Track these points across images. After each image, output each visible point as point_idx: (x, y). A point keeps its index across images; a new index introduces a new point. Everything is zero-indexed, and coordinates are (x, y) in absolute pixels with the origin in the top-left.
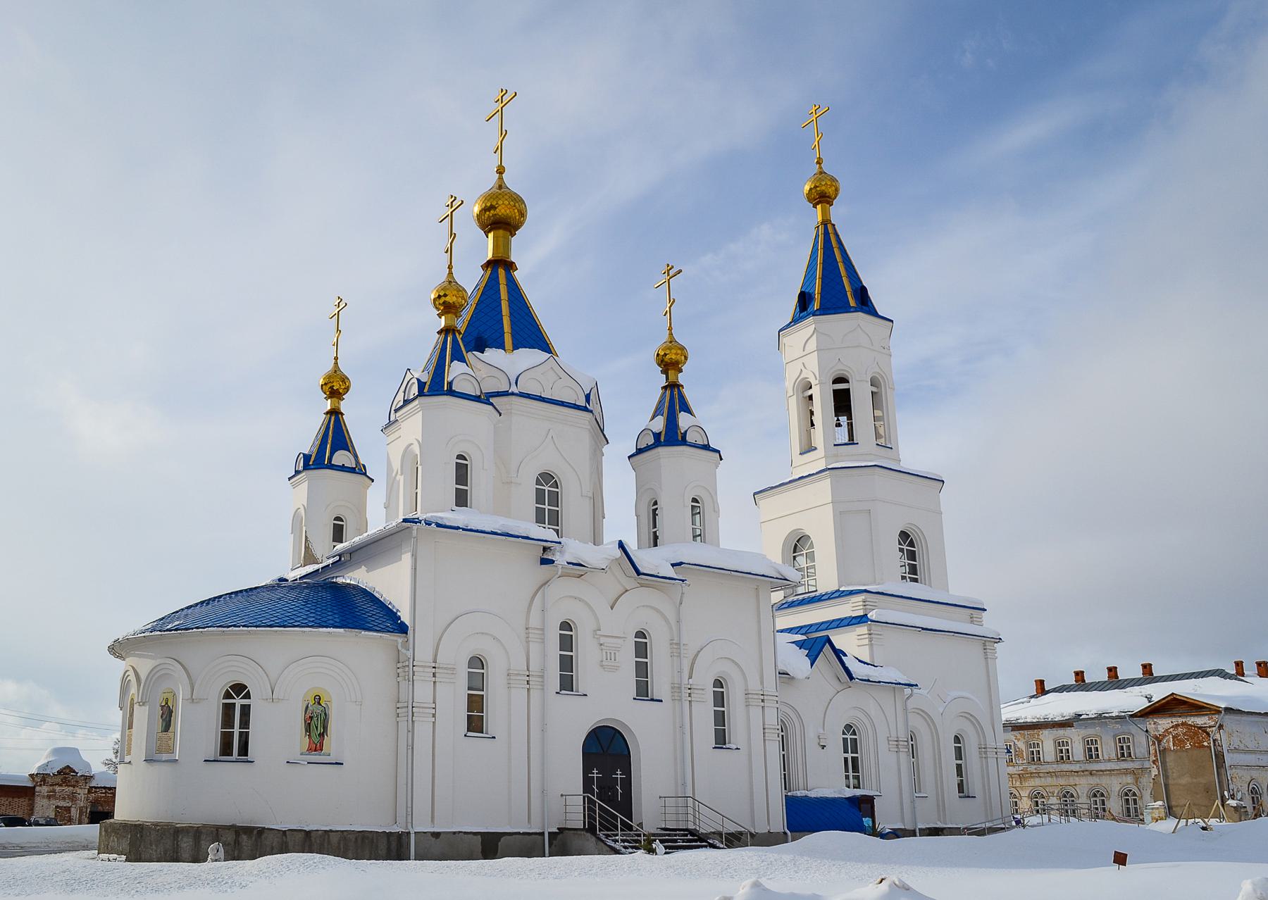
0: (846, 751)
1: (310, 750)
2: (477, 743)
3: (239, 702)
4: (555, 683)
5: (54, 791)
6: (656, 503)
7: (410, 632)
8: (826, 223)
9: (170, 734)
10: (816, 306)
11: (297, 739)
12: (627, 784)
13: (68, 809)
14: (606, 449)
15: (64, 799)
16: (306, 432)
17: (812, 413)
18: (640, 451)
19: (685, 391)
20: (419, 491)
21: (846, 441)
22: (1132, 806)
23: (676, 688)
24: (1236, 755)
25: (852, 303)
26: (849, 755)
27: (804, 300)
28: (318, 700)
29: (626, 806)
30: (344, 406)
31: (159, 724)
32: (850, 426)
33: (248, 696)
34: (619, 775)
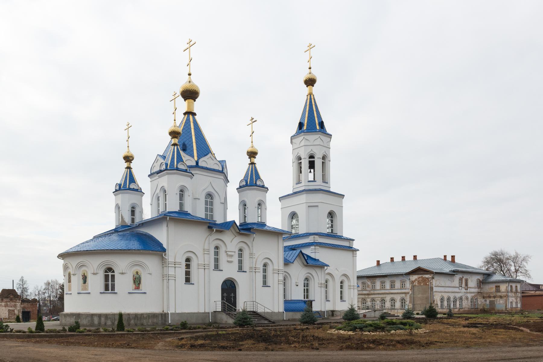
0: (304, 287)
1: (135, 288)
2: (189, 286)
3: (110, 274)
4: (212, 266)
5: (7, 304)
6: (245, 205)
7: (167, 251)
8: (310, 94)
9: (86, 284)
10: (305, 128)
11: (131, 286)
12: (235, 298)
13: (14, 311)
14: (228, 184)
15: (11, 307)
16: (119, 176)
17: (301, 167)
18: (241, 187)
19: (256, 165)
20: (167, 202)
21: (313, 180)
22: (403, 304)
23: (251, 268)
24: (437, 288)
25: (318, 127)
26: (306, 288)
27: (301, 125)
28: (137, 273)
29: (235, 304)
30: (132, 165)
31: (81, 281)
32: (314, 171)
33: (113, 272)
34: (232, 295)
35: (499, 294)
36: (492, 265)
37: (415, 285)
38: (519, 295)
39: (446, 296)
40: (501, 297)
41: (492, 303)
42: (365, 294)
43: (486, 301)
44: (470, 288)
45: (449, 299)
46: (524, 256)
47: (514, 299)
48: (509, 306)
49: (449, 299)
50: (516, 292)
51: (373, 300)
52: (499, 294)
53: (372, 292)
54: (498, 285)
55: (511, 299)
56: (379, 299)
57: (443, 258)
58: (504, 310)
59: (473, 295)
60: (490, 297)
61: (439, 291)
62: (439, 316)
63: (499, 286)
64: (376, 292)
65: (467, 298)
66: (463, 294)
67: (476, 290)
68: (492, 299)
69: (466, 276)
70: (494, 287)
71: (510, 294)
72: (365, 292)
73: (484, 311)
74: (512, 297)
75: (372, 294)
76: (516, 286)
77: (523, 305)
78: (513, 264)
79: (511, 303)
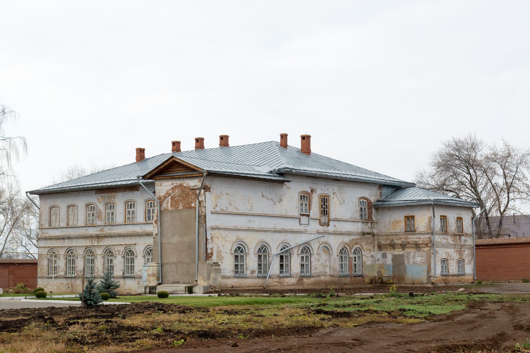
35: (413, 238)
36: (455, 175)
37: (166, 210)
38: (470, 242)
39: (252, 242)
40: (417, 246)
41: (398, 262)
42: (91, 237)
43: (384, 256)
44: (336, 220)
45: (263, 251)
46: (523, 152)
47: (451, 251)
48: (438, 271)
49: (263, 251)
50: (460, 233)
51: (109, 252)
52: (413, 238)
53: (107, 230)
54: (410, 213)
55: (442, 253)
56: (122, 249)
57: (279, 140)
58: (425, 281)
59: (347, 239)
60: (393, 246)
61: (231, 225)
62: (170, 295)
63: (413, 217)
64: (116, 230)
65: (327, 249)
66: (312, 237)
67: (358, 227)
68: (398, 252)
69: (321, 189)
70: (402, 218)
71: (437, 238)
72: (92, 231)
73: (379, 284)
74: (446, 246)
75: (106, 237)
76: (460, 219)
77: (479, 269)
78: (500, 171)
79: (444, 261)
